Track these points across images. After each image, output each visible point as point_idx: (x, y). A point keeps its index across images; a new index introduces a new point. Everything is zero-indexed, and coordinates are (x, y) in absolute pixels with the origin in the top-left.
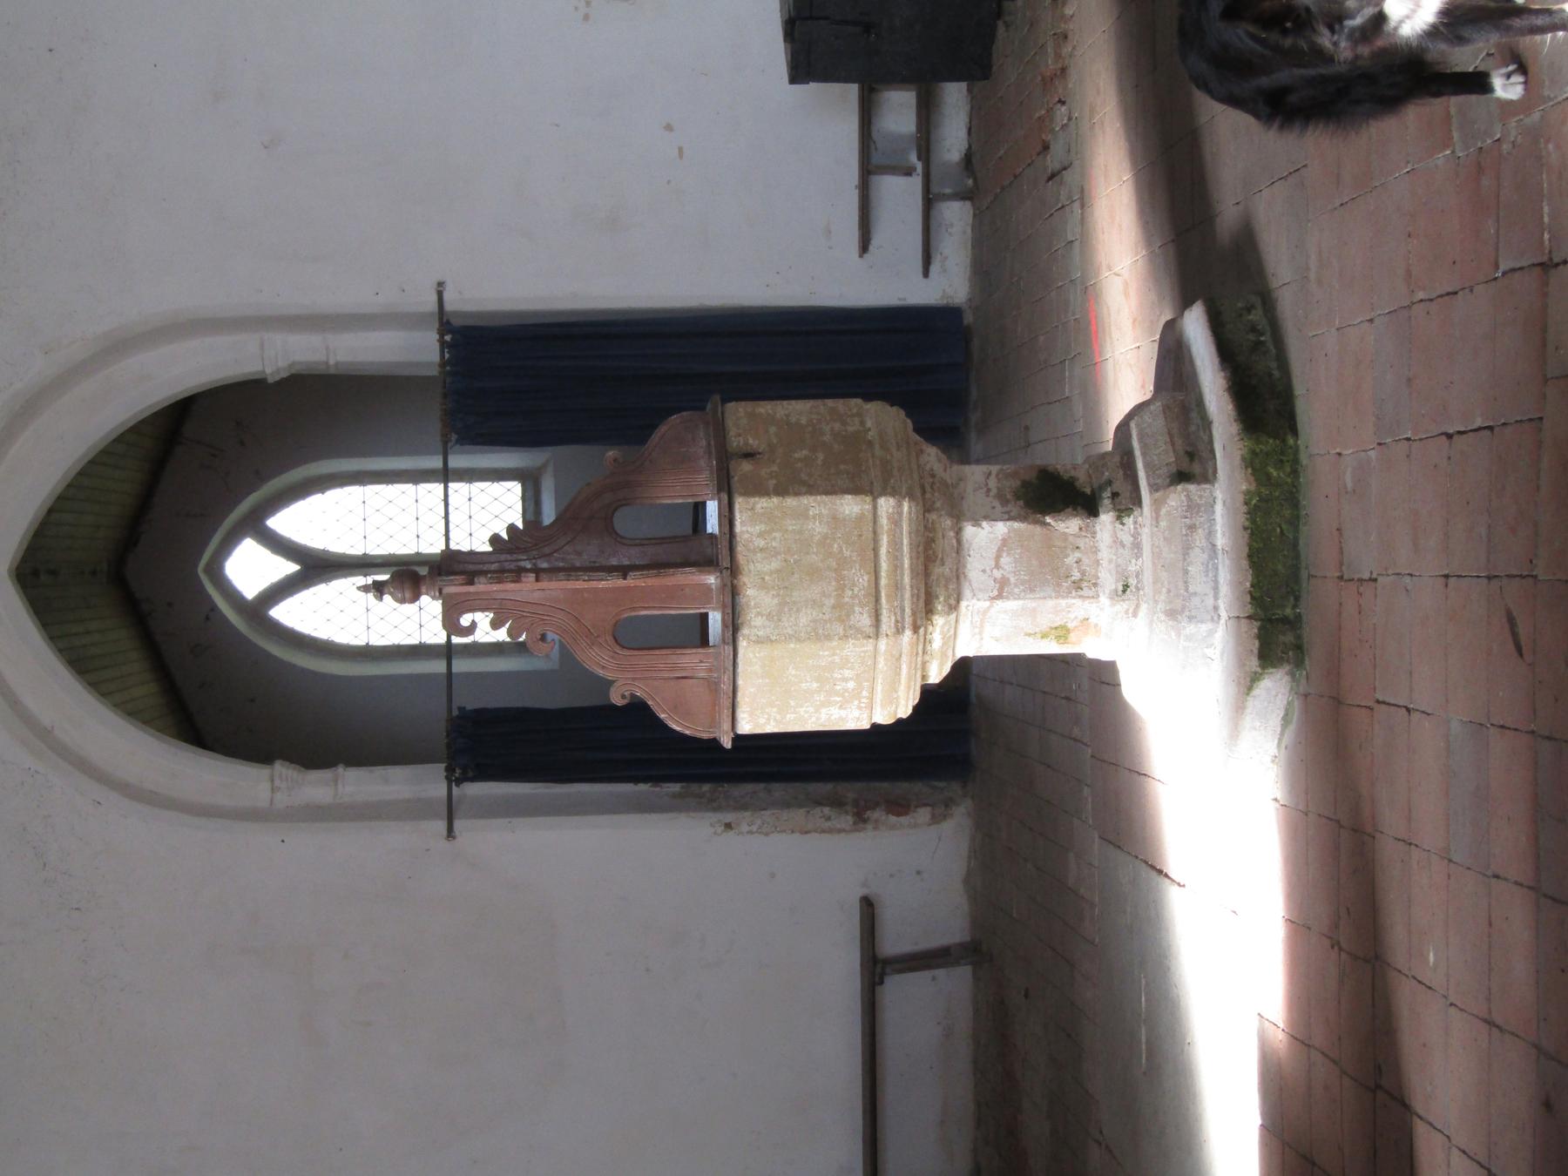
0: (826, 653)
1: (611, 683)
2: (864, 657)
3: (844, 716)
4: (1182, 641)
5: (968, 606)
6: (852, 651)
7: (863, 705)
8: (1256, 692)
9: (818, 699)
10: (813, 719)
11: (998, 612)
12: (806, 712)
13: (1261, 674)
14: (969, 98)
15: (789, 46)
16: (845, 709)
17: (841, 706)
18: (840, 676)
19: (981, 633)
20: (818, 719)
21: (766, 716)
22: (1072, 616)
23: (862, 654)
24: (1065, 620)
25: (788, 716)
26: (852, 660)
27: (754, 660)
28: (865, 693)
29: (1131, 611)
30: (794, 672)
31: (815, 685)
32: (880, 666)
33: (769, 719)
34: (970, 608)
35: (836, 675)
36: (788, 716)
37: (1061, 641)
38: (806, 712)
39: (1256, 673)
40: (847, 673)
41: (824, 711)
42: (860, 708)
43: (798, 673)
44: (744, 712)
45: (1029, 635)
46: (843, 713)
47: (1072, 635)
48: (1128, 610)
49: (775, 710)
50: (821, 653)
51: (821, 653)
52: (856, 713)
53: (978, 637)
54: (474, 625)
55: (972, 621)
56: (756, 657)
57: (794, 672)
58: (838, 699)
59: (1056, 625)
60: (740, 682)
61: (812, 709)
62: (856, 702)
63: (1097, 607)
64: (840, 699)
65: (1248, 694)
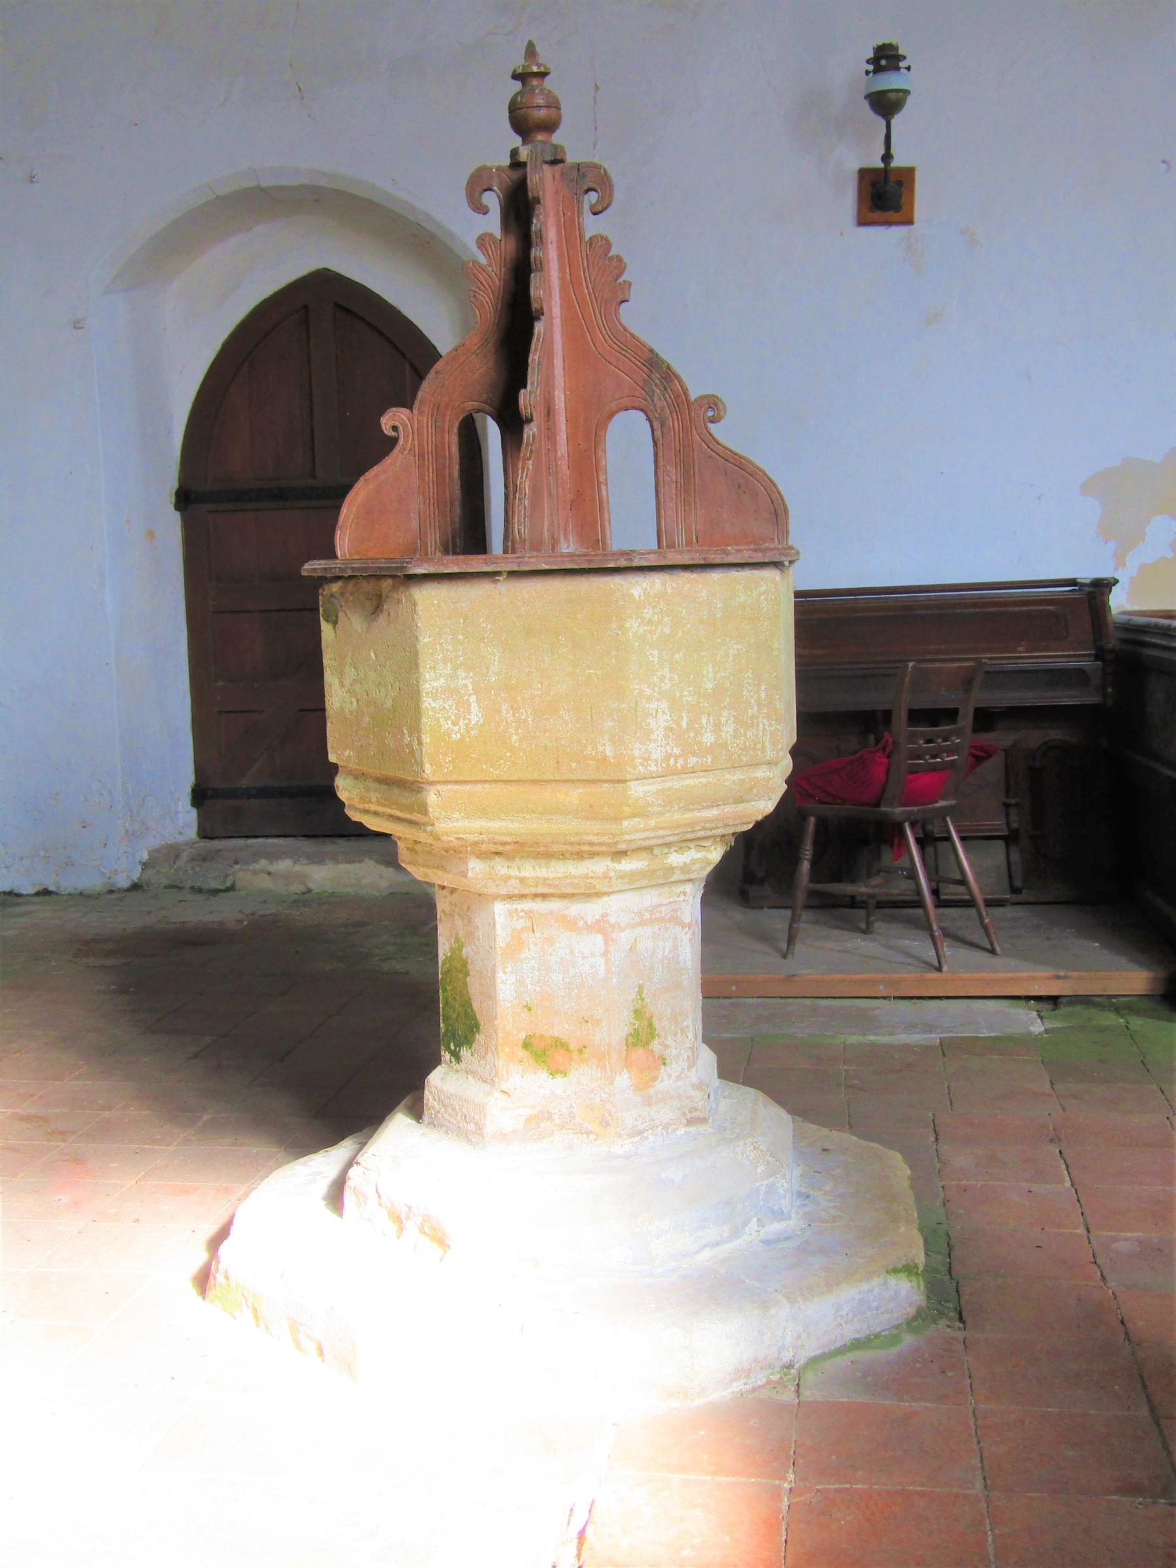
0: (763, 695)
1: (411, 409)
2: (755, 749)
3: (652, 737)
5: (685, 894)
6: (764, 729)
7: (672, 761)
8: (892, 1280)
9: (686, 693)
10: (648, 692)
11: (675, 938)
12: (662, 678)
13: (917, 1274)
14: (73, 891)
15: (1106, 599)
16: (666, 737)
17: (672, 729)
18: (723, 720)
20: (649, 699)
21: (656, 618)
22: (669, 1042)
23: (759, 746)
24: (663, 1033)
25: (656, 652)
26: (749, 734)
27: (755, 593)
28: (692, 761)
29: (696, 1114)
30: (732, 652)
31: (709, 686)
32: (727, 776)
33: (650, 622)
34: (682, 898)
35: (725, 713)
36: (656, 652)
37: (631, 1040)
38: (708, 672)
39: (916, 1266)
40: (728, 730)
41: (664, 705)
42: (668, 757)
43: (731, 658)
44: (664, 584)
45: (640, 992)
46: (658, 735)
47: (641, 1051)
48: (696, 1110)
49: (667, 630)
50: (763, 688)
51: (763, 688)
53: (637, 920)
55: (661, 905)
56: (760, 595)
57: (732, 652)
58: (684, 724)
60: (716, 576)
61: (666, 686)
62: (676, 751)
63: (683, 1069)
64: (684, 726)
65: (888, 1272)
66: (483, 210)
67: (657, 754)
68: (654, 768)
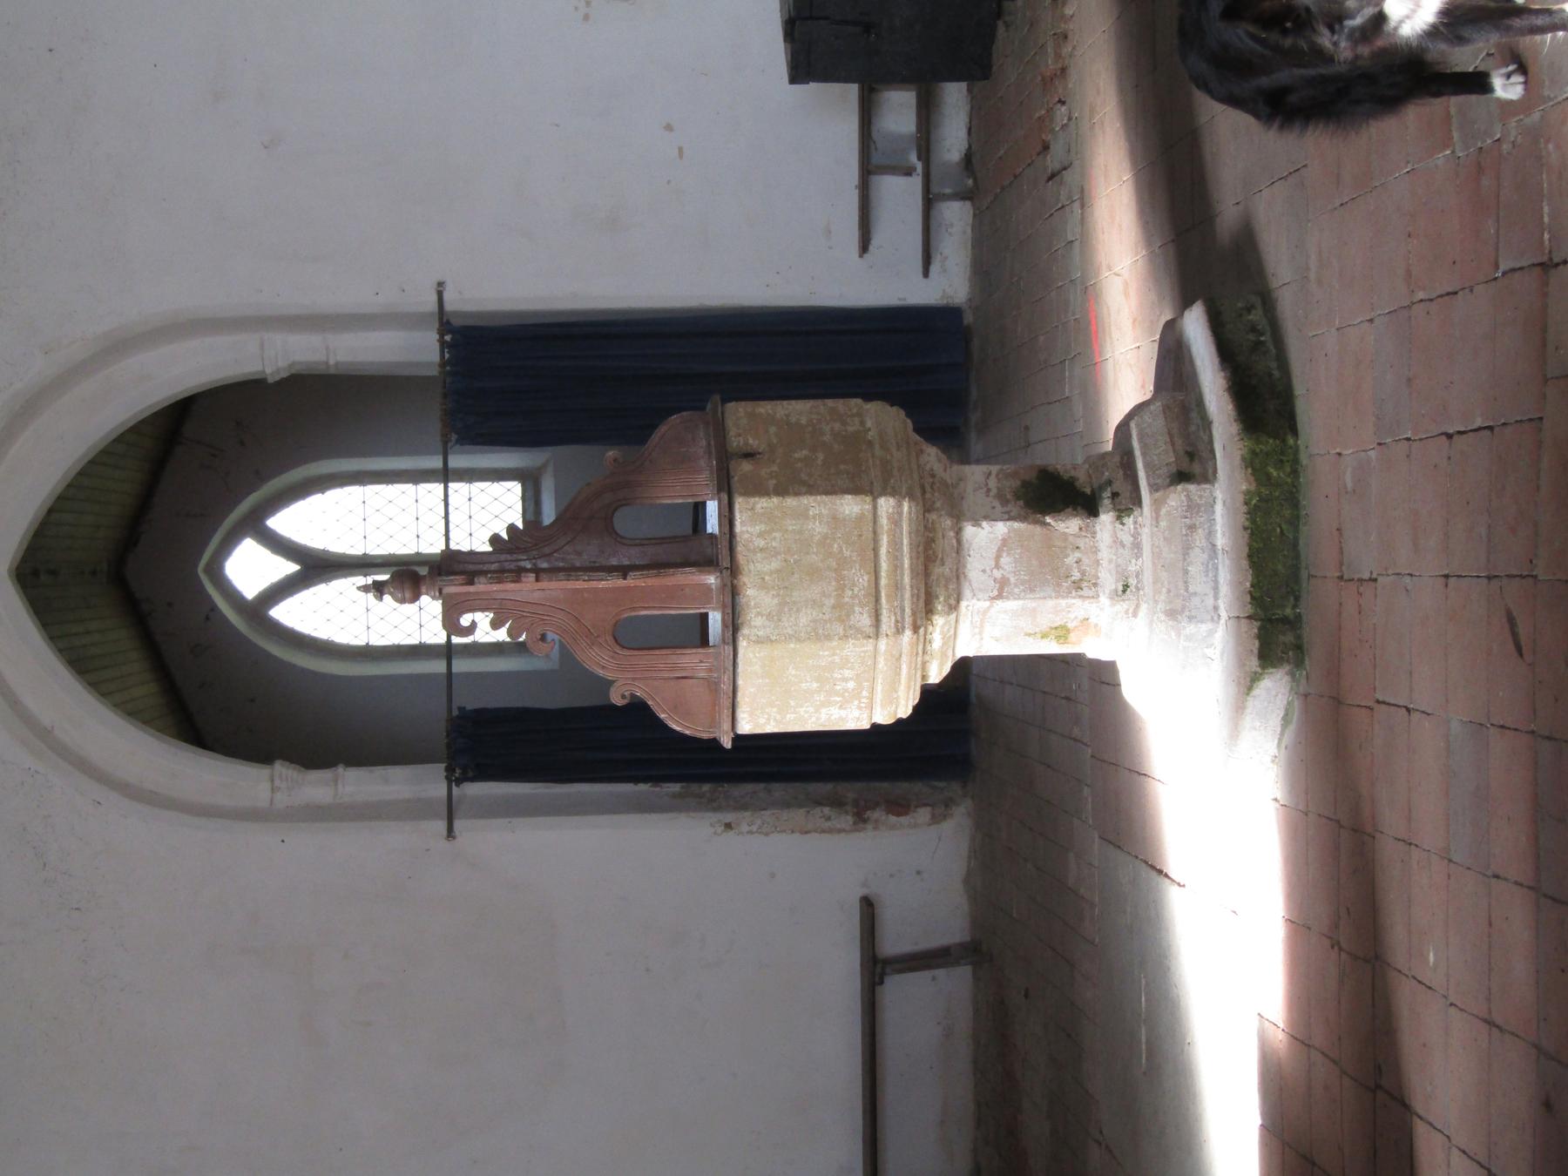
0: (826, 653)
1: (611, 683)
3: (844, 716)
6: (852, 651)
7: (863, 705)
8: (1256, 692)
9: (818, 699)
10: (813, 719)
11: (998, 612)
12: (806, 712)
13: (1261, 674)
15: (789, 46)
16: (845, 709)
17: (841, 706)
18: (840, 676)
20: (818, 719)
21: (766, 716)
22: (1072, 616)
23: (862, 654)
24: (1065, 620)
25: (788, 716)
26: (852, 660)
27: (754, 660)
28: (865, 693)
29: (1131, 611)
30: (794, 672)
31: (815, 685)
33: (769, 719)
34: (970, 608)
35: (836, 675)
37: (1061, 641)
38: (806, 712)
39: (1256, 673)
40: (847, 673)
41: (824, 711)
42: (860, 708)
43: (798, 673)
44: (744, 712)
45: (1029, 635)
46: (843, 713)
47: (1072, 635)
48: (1128, 610)
49: (775, 710)
50: (821, 653)
51: (821, 653)
53: (978, 637)
56: (756, 657)
57: (794, 672)
58: (838, 699)
59: (1056, 625)
60: (740, 682)
61: (812, 709)
62: (856, 702)
63: (1097, 607)
64: (840, 699)
65: (1248, 694)
66: (474, 625)
67: (856, 713)
68: (865, 716)
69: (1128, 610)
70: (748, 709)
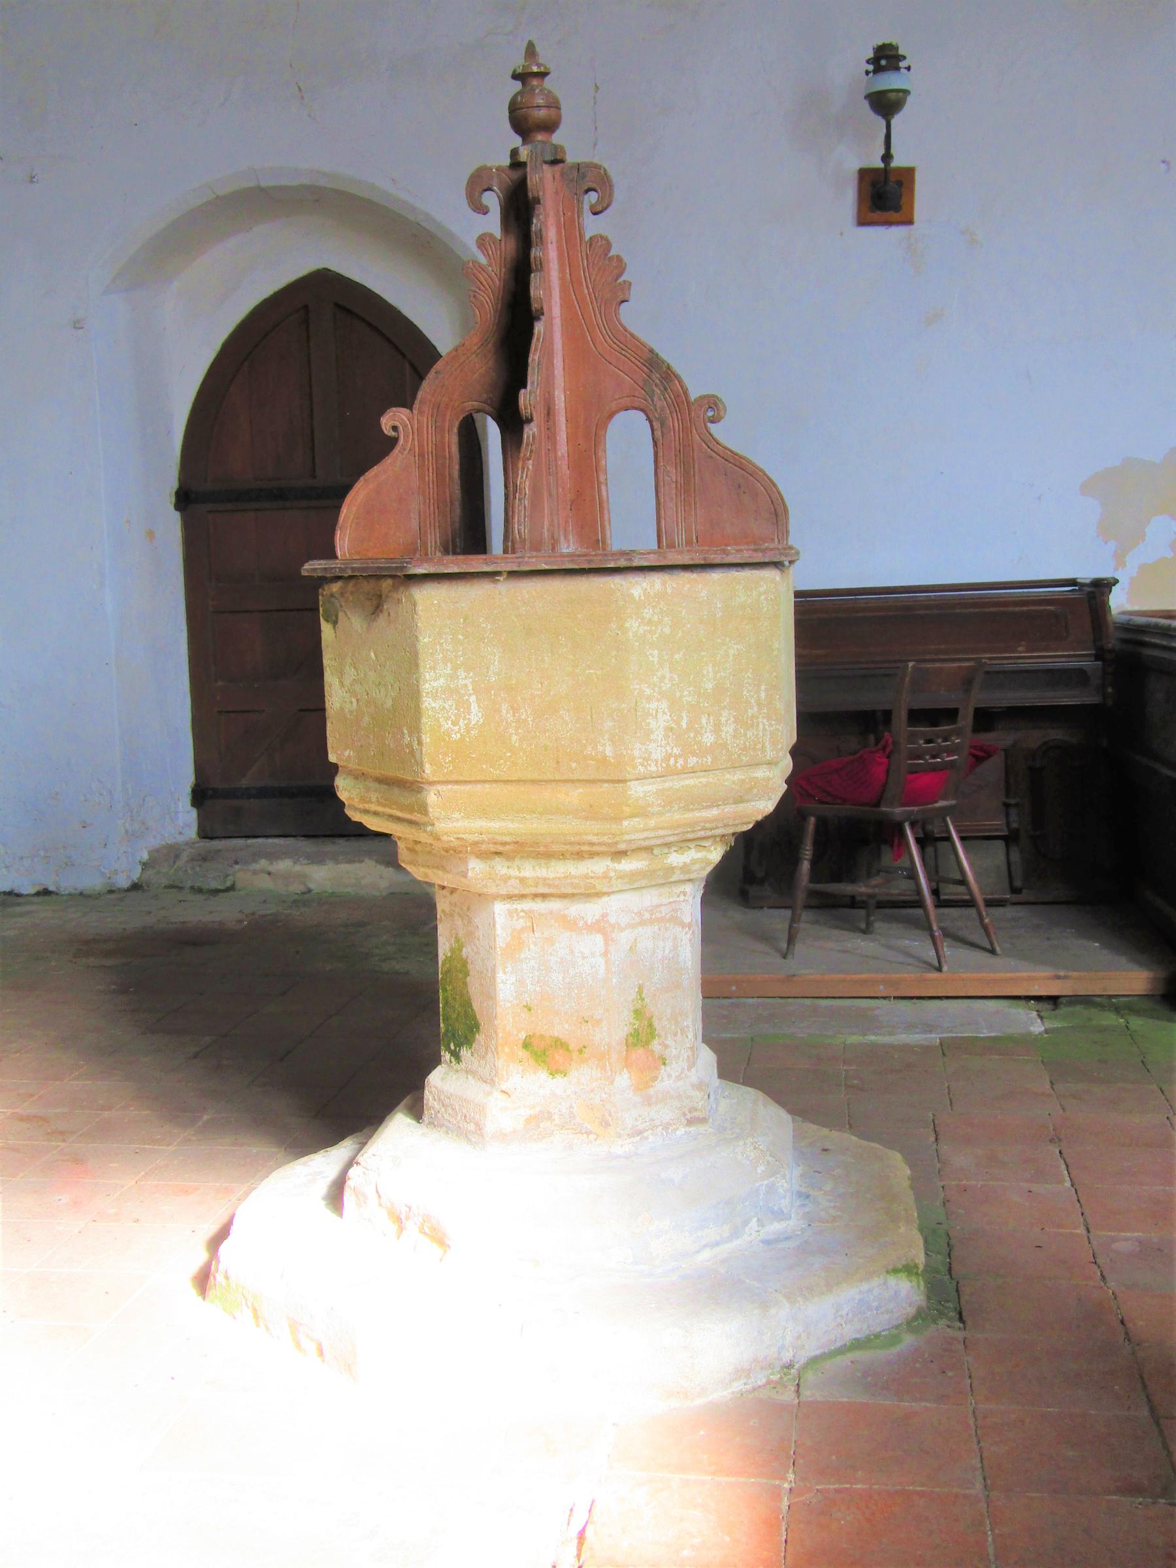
0: (763, 695)
1: (411, 409)
3: (652, 737)
4: (765, 1182)
6: (764, 729)
7: (672, 761)
8: (892, 1280)
9: (686, 693)
10: (648, 692)
11: (675, 938)
12: (662, 678)
13: (917, 1274)
15: (1106, 599)
16: (666, 737)
17: (672, 729)
18: (723, 720)
19: (643, 923)
20: (649, 699)
21: (656, 618)
22: (669, 1042)
23: (759, 746)
24: (663, 1033)
25: (656, 652)
26: (749, 734)
27: (755, 593)
28: (692, 761)
29: (696, 1114)
30: (732, 652)
31: (709, 686)
33: (650, 622)
34: (682, 898)
35: (725, 713)
37: (631, 1040)
38: (708, 672)
39: (916, 1266)
40: (728, 730)
41: (664, 705)
42: (668, 757)
43: (731, 658)
44: (664, 584)
45: (640, 992)
46: (658, 735)
47: (641, 1051)
48: (696, 1110)
49: (667, 630)
50: (763, 688)
51: (763, 688)
52: (657, 754)
53: (637, 920)
54: (483, 210)
56: (760, 595)
57: (732, 652)
58: (684, 724)
59: (656, 1024)
60: (716, 576)
62: (676, 751)
63: (683, 1069)
64: (684, 726)
65: (888, 1272)
66: (483, 210)
69: (696, 1110)
70: (669, 591)
